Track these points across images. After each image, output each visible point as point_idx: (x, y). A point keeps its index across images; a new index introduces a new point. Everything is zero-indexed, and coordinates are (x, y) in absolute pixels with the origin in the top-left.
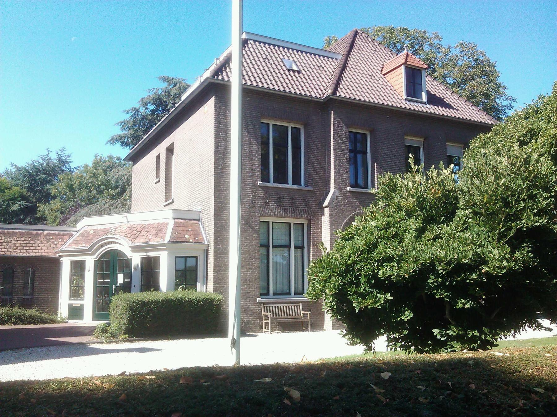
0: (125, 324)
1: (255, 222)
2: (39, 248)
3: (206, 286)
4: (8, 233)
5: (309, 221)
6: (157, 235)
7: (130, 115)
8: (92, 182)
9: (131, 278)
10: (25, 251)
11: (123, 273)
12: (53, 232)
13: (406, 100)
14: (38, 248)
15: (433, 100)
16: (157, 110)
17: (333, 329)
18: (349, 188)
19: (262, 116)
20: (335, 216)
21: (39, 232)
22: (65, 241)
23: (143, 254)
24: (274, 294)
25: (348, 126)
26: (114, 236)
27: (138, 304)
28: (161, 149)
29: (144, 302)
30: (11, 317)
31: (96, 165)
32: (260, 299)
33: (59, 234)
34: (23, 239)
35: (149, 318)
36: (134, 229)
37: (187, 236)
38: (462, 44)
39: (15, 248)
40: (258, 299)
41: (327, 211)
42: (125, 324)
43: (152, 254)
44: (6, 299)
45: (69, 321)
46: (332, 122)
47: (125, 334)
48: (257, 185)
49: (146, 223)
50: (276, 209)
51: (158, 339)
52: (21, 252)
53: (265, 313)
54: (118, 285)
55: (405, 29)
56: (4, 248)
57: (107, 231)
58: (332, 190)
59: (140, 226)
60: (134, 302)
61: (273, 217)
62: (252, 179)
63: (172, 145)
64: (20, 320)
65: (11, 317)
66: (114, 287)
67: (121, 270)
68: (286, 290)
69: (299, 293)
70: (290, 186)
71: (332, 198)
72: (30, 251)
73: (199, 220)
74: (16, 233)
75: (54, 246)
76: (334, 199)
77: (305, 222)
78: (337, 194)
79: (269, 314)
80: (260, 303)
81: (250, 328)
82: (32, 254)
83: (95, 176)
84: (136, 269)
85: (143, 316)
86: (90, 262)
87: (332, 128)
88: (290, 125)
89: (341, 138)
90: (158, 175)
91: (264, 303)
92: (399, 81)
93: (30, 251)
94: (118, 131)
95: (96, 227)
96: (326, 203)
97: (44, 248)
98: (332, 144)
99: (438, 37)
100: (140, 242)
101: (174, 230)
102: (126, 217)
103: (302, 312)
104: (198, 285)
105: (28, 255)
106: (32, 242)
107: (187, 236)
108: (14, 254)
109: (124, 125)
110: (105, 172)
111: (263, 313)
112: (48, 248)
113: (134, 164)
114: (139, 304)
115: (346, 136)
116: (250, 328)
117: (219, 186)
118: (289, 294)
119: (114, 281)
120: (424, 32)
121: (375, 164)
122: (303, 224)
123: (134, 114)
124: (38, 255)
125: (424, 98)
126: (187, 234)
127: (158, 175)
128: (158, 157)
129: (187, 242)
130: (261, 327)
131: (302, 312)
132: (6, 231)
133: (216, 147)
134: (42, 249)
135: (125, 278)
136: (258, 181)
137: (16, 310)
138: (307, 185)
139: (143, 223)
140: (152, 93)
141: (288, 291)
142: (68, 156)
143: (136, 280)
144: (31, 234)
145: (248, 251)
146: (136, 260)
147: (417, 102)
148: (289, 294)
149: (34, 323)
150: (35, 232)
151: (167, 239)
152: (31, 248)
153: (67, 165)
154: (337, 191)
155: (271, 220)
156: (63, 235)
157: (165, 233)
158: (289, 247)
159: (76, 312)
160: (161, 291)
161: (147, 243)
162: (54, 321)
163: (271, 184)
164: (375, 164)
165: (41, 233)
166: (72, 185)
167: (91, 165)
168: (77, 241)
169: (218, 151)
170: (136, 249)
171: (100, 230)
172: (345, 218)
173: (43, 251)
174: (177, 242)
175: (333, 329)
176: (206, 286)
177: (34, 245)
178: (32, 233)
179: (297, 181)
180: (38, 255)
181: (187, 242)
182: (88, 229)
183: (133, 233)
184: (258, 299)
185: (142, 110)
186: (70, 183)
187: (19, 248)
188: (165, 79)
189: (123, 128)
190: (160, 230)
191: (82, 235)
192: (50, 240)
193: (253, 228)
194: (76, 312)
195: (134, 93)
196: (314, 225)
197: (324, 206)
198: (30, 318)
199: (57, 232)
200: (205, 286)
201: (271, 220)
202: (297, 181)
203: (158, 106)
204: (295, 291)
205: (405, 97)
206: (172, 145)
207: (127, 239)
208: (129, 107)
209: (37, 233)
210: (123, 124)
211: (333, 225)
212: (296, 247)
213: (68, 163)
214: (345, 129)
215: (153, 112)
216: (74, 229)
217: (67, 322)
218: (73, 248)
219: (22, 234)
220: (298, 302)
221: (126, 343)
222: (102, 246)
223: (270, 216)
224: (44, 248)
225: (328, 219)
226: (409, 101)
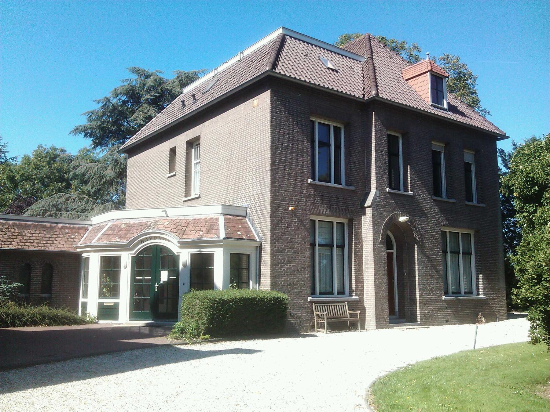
0: (204, 324)
1: (306, 220)
2: (57, 242)
3: (259, 285)
4: (21, 225)
5: (351, 221)
6: (208, 231)
7: (101, 105)
8: (36, 175)
9: (178, 276)
10: (42, 245)
11: (168, 271)
12: (67, 225)
13: (431, 106)
14: (55, 242)
15: (452, 108)
16: (128, 102)
17: (377, 329)
18: (388, 190)
19: (312, 114)
20: (377, 216)
21: (54, 225)
22: (82, 235)
23: (195, 251)
24: (320, 293)
25: (387, 128)
26: (158, 231)
27: (218, 302)
28: (180, 141)
29: (223, 300)
30: (45, 317)
31: (39, 156)
32: (311, 298)
33: (74, 228)
34: (37, 232)
35: (228, 317)
36: (178, 224)
37: (239, 233)
38: (448, 56)
39: (32, 241)
40: (309, 299)
41: (369, 211)
42: (204, 324)
43: (206, 251)
44: (45, 297)
45: (100, 321)
46: (374, 123)
47: (204, 334)
48: (308, 183)
49: (191, 218)
50: (323, 208)
51: (249, 339)
52: (38, 246)
53: (318, 313)
54: (161, 282)
55: (383, 38)
56: (20, 242)
57: (145, 226)
58: (373, 191)
59: (184, 221)
60: (214, 301)
61: (321, 215)
62: (304, 176)
63: (198, 138)
64: (54, 320)
65: (45, 317)
66: (157, 285)
67: (164, 267)
68: (328, 289)
69: (341, 292)
70: (332, 184)
71: (374, 199)
72: (49, 245)
73: (245, 217)
74: (29, 226)
75: (72, 240)
76: (376, 199)
77: (345, 221)
78: (378, 195)
79: (325, 313)
80: (311, 303)
81: (303, 327)
82: (52, 249)
83: (37, 167)
84: (185, 266)
85: (223, 315)
86: (126, 259)
87: (373, 129)
88: (332, 124)
89: (381, 139)
90: (172, 168)
91: (316, 302)
92: (424, 87)
93: (49, 245)
94: (83, 121)
95: (127, 221)
96: (368, 203)
97: (62, 243)
98: (373, 145)
99: (416, 48)
100: (190, 237)
101: (226, 227)
102: (166, 211)
103: (348, 312)
104: (251, 283)
105: (47, 249)
106: (48, 236)
107: (239, 233)
108: (32, 248)
109: (91, 115)
110: (49, 163)
111: (315, 313)
112: (66, 242)
113: (129, 158)
114: (219, 303)
115: (385, 137)
116: (303, 327)
117: (275, 182)
118: (332, 293)
119: (157, 277)
120: (404, 42)
121: (409, 167)
122: (343, 224)
123: (105, 104)
124: (57, 249)
125: (445, 106)
126: (239, 231)
127: (172, 168)
128: (173, 151)
129: (241, 239)
130: (313, 327)
131: (348, 312)
132: (18, 222)
133: (272, 142)
134: (60, 243)
135: (169, 276)
136: (308, 178)
137: (45, 309)
138: (348, 184)
139: (187, 218)
140: (126, 84)
141: (330, 290)
142: (4, 146)
143: (185, 279)
144: (45, 227)
145: (301, 249)
146: (185, 257)
147: (438, 108)
148: (332, 293)
149: (68, 324)
150: (48, 225)
151: (222, 235)
152: (49, 242)
153: (3, 155)
154: (378, 192)
155: (317, 218)
156: (79, 228)
157: (218, 229)
158: (332, 246)
159: (108, 312)
160: (217, 288)
161: (199, 238)
162: (76, 322)
163: (317, 182)
164: (409, 167)
165: (55, 226)
166: (14, 177)
167: (32, 157)
168: (97, 235)
169: (274, 146)
170: (184, 245)
171: (134, 224)
172: (385, 219)
173: (62, 246)
174: (231, 238)
175: (377, 329)
176: (259, 285)
177: (51, 239)
178: (45, 225)
179: (338, 181)
180: (57, 249)
181: (241, 239)
182: (119, 222)
183: (180, 227)
184: (309, 299)
185: (114, 101)
186: (11, 174)
187: (36, 241)
188: (137, 71)
189: (90, 119)
190: (211, 226)
191: (110, 229)
192: (66, 234)
193: (304, 226)
194: (108, 312)
195: (106, 83)
196: (355, 224)
197: (365, 205)
198: (63, 318)
199: (72, 226)
200: (258, 284)
201: (317, 218)
202: (338, 181)
203: (131, 97)
204: (320, 290)
205: (430, 103)
206: (198, 138)
207: (174, 234)
208: (101, 97)
209: (51, 226)
210: (90, 114)
211: (375, 224)
212: (338, 246)
213: (4, 153)
214: (384, 131)
215: (124, 103)
216: (90, 223)
217: (97, 323)
218: (105, 242)
219: (35, 227)
220: (343, 302)
221: (209, 344)
222: (142, 241)
223: (319, 214)
224: (62, 243)
225: (371, 219)
226: (435, 107)
